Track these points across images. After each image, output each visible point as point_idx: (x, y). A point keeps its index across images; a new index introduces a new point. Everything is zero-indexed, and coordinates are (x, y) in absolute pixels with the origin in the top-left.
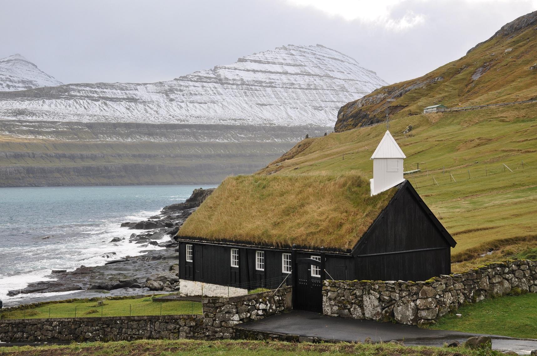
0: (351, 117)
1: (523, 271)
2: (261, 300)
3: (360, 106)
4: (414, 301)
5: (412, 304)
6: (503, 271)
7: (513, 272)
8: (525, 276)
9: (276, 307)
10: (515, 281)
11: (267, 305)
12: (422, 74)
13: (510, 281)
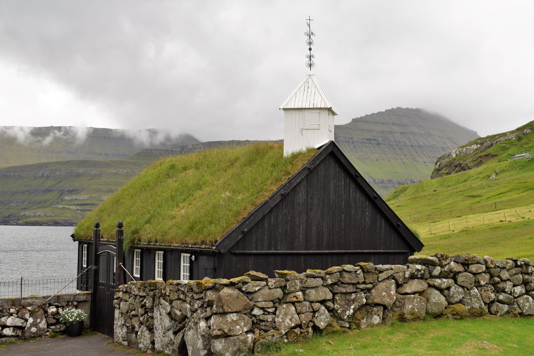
0: (446, 166)
1: (475, 274)
2: (12, 310)
3: (454, 156)
4: (207, 319)
5: (202, 324)
6: (430, 273)
7: (454, 276)
8: (478, 285)
9: (49, 325)
10: (457, 292)
11: (26, 320)
12: (514, 128)
13: (446, 292)
